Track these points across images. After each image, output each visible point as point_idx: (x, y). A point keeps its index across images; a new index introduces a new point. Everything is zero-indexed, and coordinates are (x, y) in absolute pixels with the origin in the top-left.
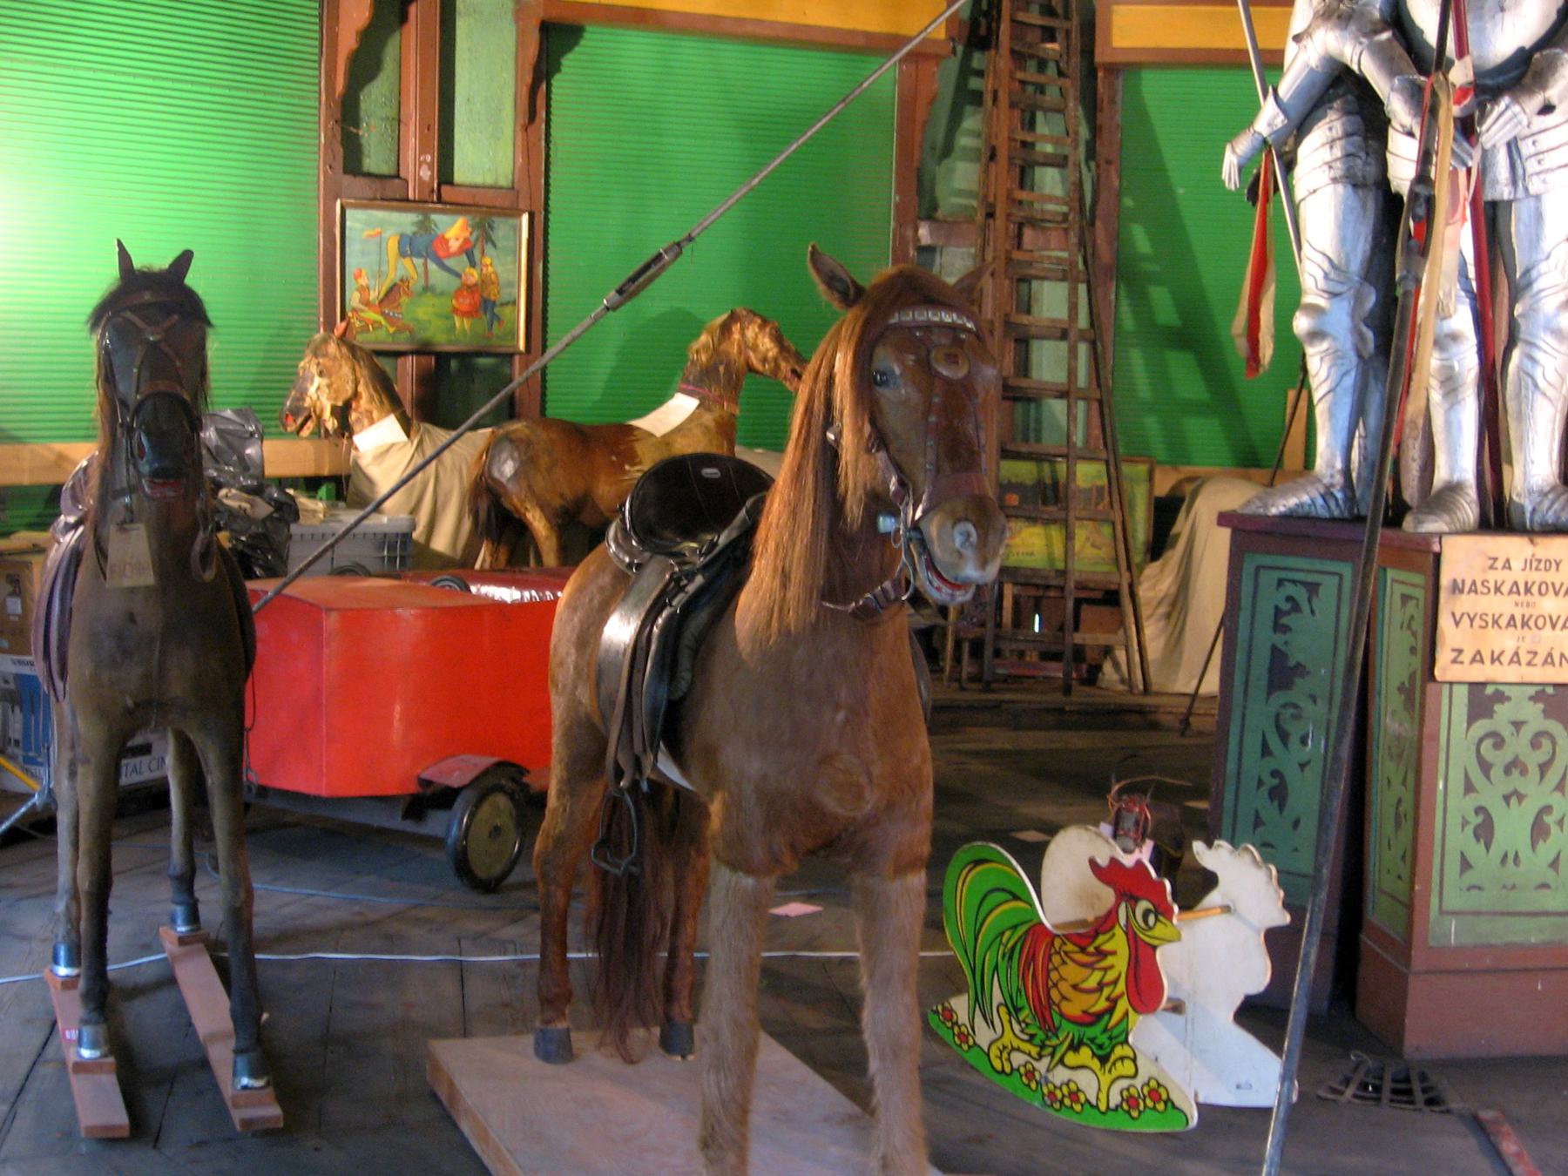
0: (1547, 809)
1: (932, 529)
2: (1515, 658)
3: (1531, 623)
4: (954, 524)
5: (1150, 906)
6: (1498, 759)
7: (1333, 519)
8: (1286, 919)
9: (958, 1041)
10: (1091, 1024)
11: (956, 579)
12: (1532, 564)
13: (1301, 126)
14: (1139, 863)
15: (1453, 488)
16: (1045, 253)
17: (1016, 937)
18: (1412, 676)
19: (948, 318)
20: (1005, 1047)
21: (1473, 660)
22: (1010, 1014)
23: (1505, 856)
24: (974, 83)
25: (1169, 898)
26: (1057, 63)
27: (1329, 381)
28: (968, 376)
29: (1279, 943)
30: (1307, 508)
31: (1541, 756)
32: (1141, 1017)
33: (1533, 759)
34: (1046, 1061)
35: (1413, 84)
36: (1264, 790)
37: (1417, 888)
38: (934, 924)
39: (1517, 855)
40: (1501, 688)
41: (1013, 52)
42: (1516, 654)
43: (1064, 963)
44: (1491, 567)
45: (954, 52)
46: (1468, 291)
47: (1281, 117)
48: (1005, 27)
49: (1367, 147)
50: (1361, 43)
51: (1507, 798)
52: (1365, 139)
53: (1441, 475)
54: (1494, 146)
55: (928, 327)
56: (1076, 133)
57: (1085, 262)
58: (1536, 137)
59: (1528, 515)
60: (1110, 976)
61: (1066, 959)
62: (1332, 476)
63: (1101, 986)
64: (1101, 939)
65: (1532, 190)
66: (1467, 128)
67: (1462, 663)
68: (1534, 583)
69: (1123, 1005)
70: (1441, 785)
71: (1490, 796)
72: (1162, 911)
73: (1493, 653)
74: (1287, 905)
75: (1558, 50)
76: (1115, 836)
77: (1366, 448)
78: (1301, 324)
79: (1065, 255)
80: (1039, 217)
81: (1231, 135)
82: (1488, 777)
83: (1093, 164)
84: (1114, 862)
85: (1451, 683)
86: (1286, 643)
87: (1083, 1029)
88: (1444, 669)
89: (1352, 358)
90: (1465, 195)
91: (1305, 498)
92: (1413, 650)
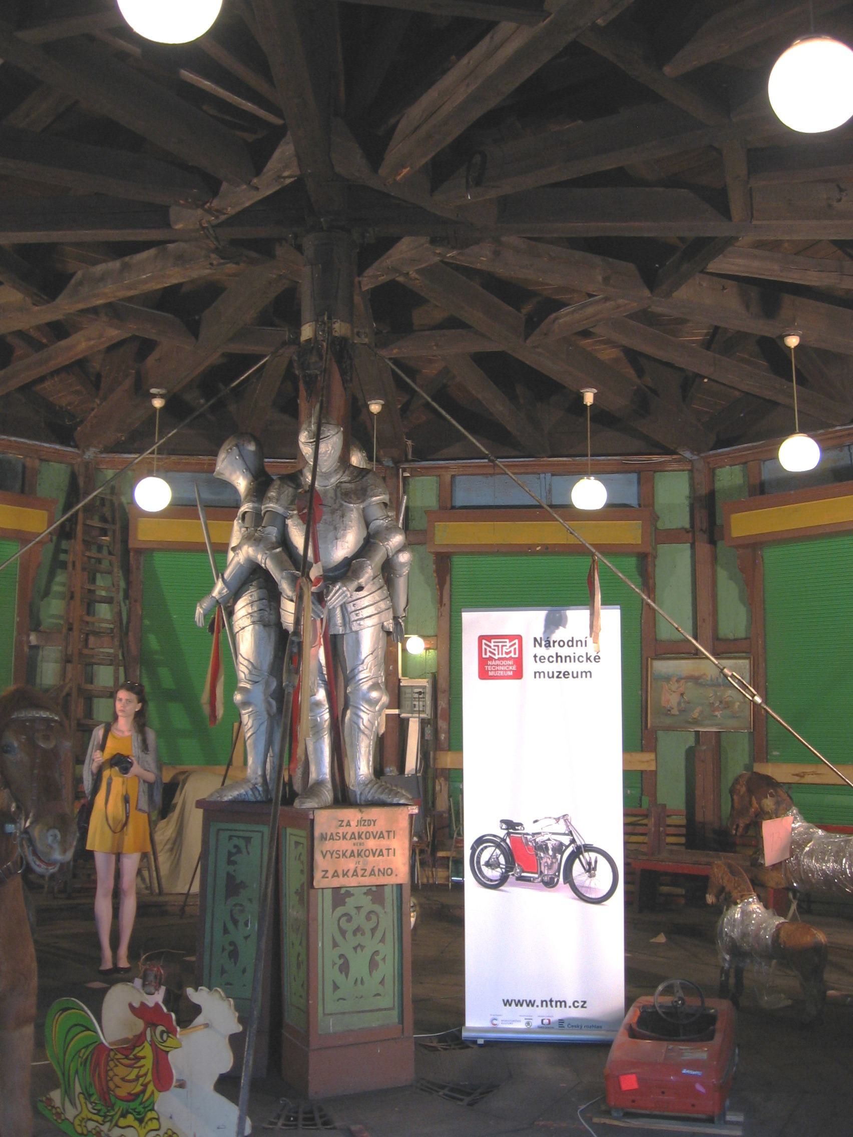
0: (376, 953)
1: (36, 833)
2: (355, 873)
3: (363, 854)
4: (48, 830)
5: (164, 1028)
6: (349, 927)
7: (257, 802)
8: (239, 1028)
9: (55, 1118)
10: (133, 1100)
11: (49, 860)
12: (361, 822)
13: (236, 595)
14: (157, 1004)
15: (319, 783)
16: (102, 650)
17: (87, 1053)
18: (302, 885)
19: (44, 714)
20: (83, 1119)
21: (333, 876)
22: (85, 1098)
23: (356, 980)
24: (62, 557)
25: (174, 1023)
26: (108, 547)
27: (253, 728)
28: (56, 746)
29: (236, 1041)
30: (244, 797)
31: (372, 924)
32: (161, 1094)
33: (367, 926)
34: (108, 1124)
35: (293, 574)
36: (226, 953)
37: (310, 1002)
38: (40, 1043)
39: (362, 979)
40: (348, 889)
41: (84, 541)
42: (355, 871)
43: (116, 1066)
44: (341, 826)
45: (51, 540)
46: (324, 681)
47: (226, 590)
48: (79, 529)
49: (270, 605)
50: (266, 554)
51: (355, 948)
52: (269, 601)
53: (313, 776)
54: (334, 608)
55: (34, 720)
56: (118, 585)
57: (123, 656)
58: (354, 603)
59: (358, 796)
60: (143, 1071)
61: (118, 1064)
62: (256, 779)
63: (138, 1077)
64: (137, 1049)
65: (354, 629)
66: (320, 598)
67: (327, 877)
68: (363, 832)
69: (151, 1087)
70: (320, 945)
71: (346, 948)
72: (171, 1031)
73: (343, 871)
74: (241, 1020)
75: (364, 559)
76: (144, 985)
77: (274, 762)
78: (238, 697)
79: (112, 651)
80: (98, 630)
81: (199, 599)
82: (344, 937)
83: (127, 602)
84: (143, 1004)
85: (323, 889)
86: (234, 871)
87: (129, 1103)
88: (319, 881)
89: (266, 716)
90: (320, 632)
91: (242, 791)
92: (302, 871)
